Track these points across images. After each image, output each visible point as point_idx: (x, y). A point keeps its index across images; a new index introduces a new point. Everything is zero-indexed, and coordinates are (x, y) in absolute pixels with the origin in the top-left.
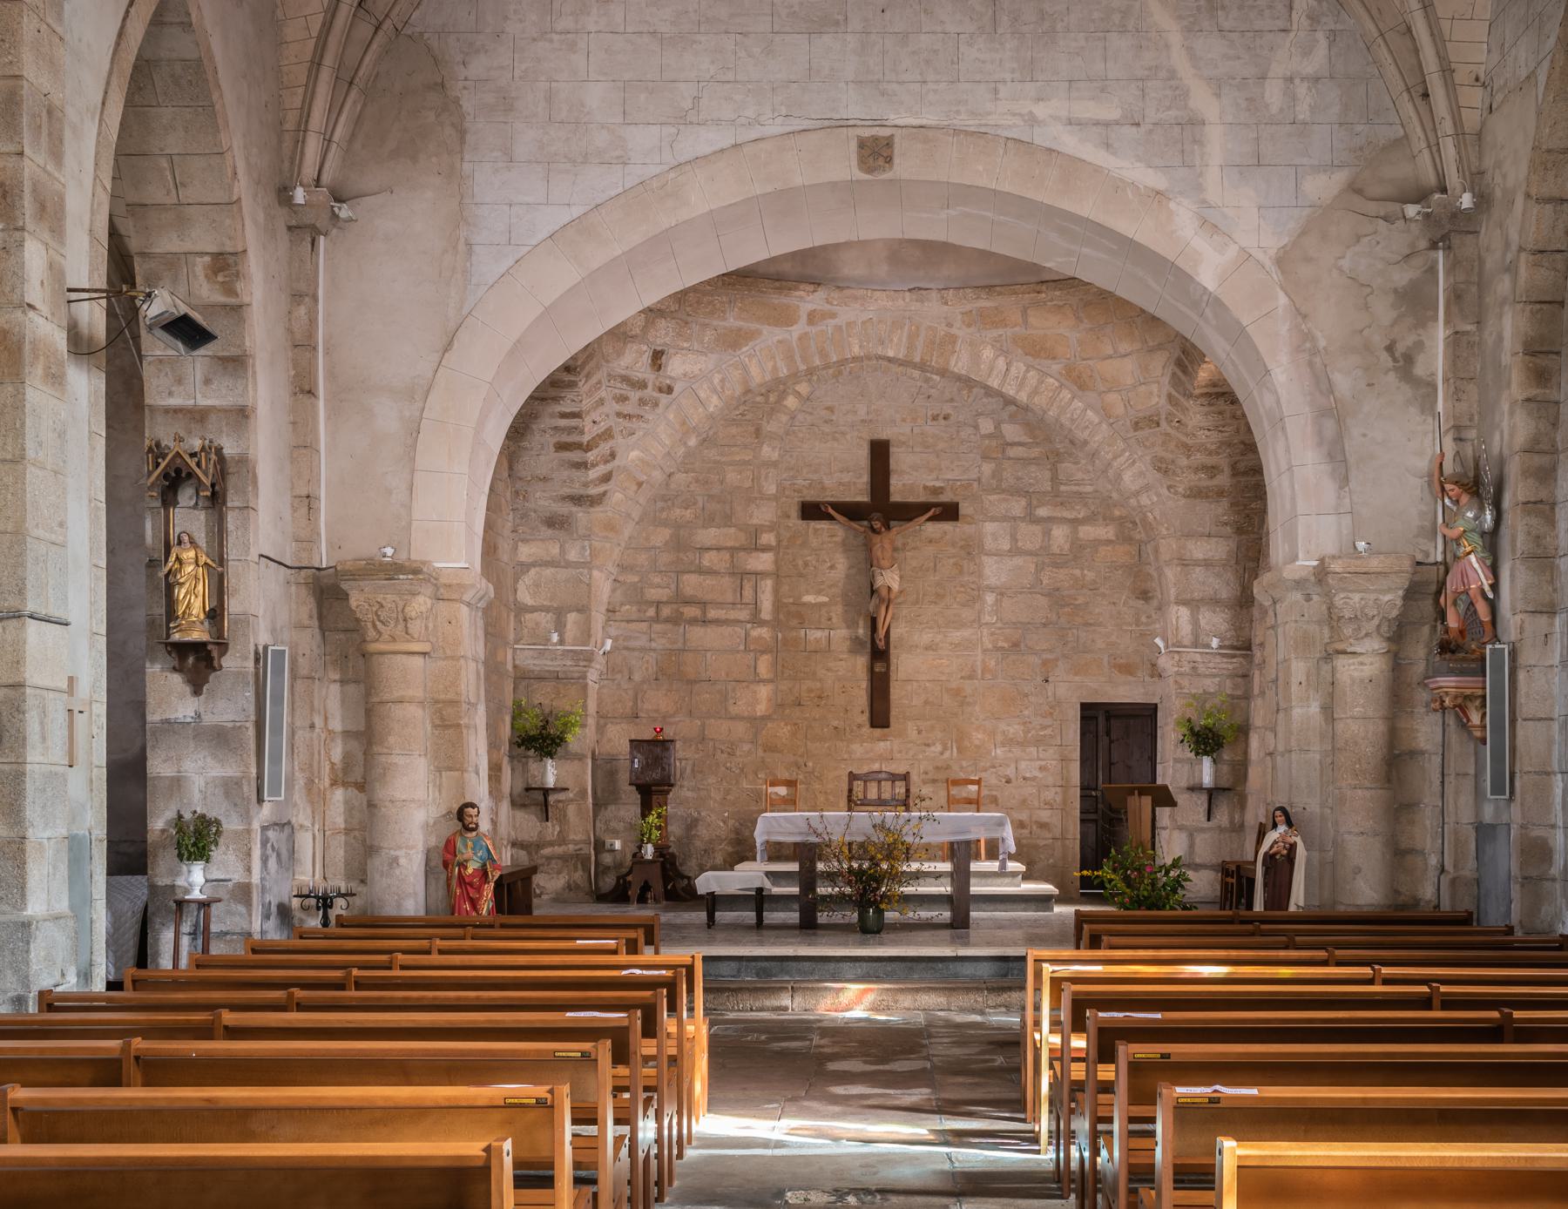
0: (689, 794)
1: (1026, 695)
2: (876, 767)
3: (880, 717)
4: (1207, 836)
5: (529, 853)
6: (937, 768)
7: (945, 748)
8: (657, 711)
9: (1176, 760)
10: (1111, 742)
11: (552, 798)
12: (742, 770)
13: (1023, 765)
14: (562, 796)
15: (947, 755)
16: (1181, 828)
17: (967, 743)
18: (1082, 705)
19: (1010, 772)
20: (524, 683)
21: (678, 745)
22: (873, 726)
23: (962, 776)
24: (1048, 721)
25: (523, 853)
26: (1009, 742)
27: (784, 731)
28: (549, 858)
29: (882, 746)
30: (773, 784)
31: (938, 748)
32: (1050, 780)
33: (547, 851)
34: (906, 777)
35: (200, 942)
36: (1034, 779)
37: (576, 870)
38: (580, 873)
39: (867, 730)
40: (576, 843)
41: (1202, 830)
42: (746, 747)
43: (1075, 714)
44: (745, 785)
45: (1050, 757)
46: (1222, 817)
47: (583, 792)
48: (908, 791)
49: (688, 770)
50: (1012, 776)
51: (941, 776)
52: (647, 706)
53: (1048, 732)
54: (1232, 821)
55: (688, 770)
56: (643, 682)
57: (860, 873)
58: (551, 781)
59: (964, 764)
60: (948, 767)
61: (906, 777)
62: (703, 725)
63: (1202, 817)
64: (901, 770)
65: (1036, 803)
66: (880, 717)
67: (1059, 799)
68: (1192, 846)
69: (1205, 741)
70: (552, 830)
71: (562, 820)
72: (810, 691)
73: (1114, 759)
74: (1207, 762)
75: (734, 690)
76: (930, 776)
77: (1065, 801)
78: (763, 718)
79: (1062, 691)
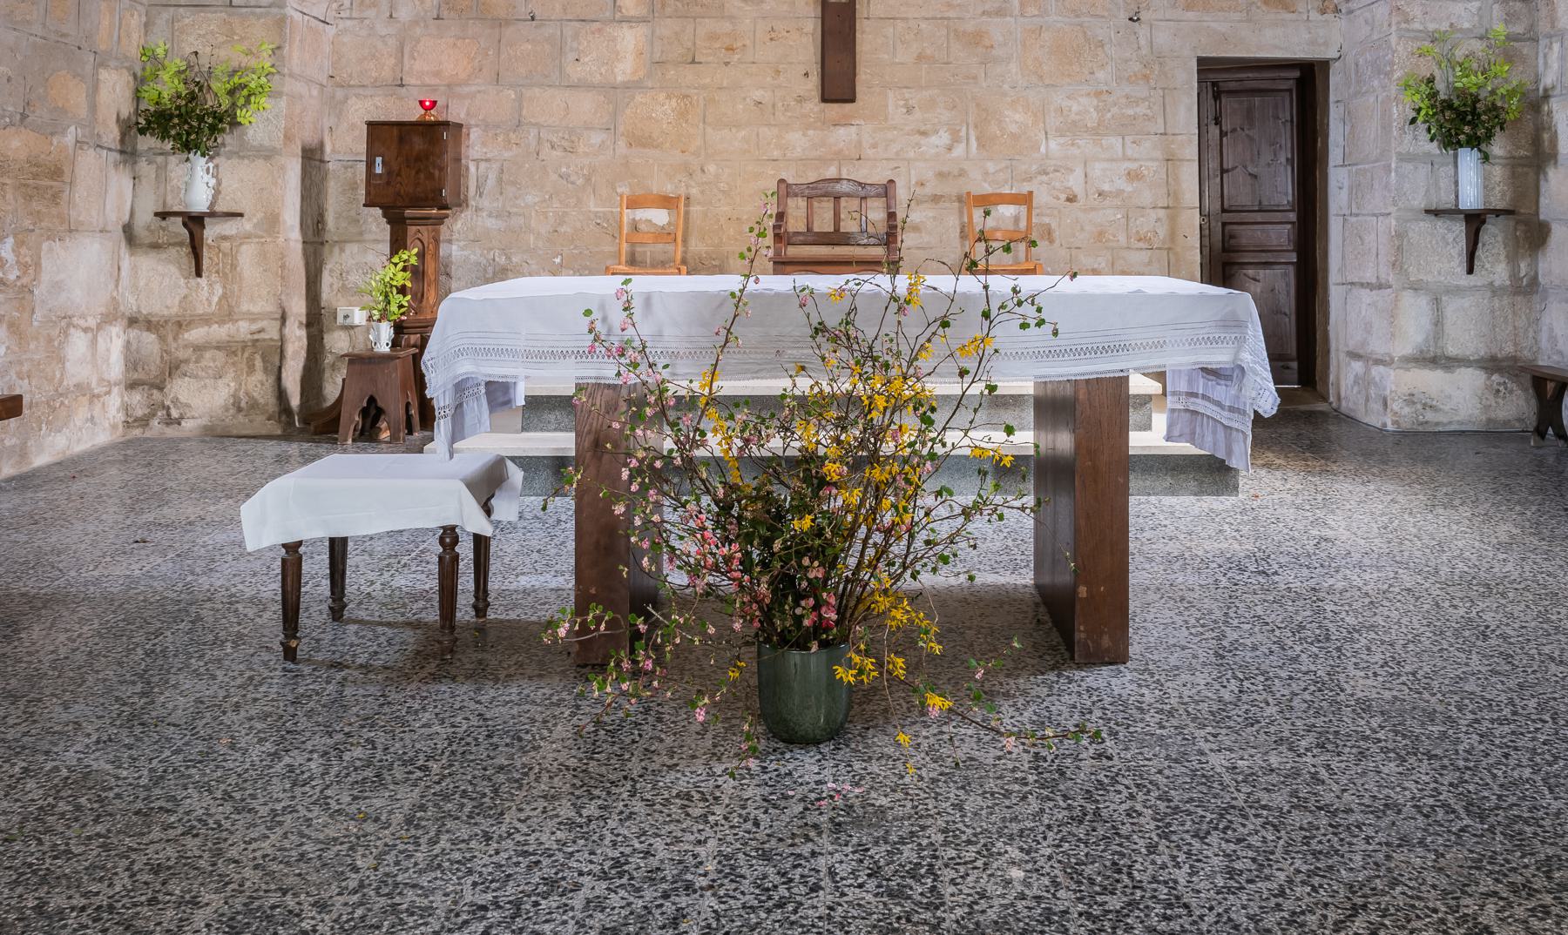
0: (491, 223)
1: (1101, 45)
2: (831, 172)
3: (838, 84)
4: (1466, 302)
5: (162, 339)
6: (941, 175)
7: (956, 139)
8: (437, 74)
9: (1405, 158)
10: (1223, 134)
11: (211, 232)
12: (588, 180)
13: (1097, 169)
14: (230, 227)
15: (959, 150)
16: (1416, 288)
17: (994, 128)
18: (1201, 61)
19: (1075, 182)
20: (166, 15)
21: (475, 134)
22: (824, 100)
23: (987, 189)
24: (1141, 90)
25: (150, 338)
26: (1072, 129)
27: (663, 109)
28: (199, 349)
29: (843, 136)
30: (634, 203)
31: (943, 138)
32: (1147, 197)
33: (196, 335)
34: (887, 191)
35: (1347, 128)
36: (1120, 192)
37: (251, 368)
38: (260, 375)
39: (814, 106)
40: (253, 318)
41: (1457, 291)
42: (596, 138)
43: (1187, 79)
44: (592, 206)
45: (1146, 153)
46: (1495, 266)
47: (272, 222)
48: (892, 216)
49: (491, 182)
50: (1078, 189)
51: (951, 188)
52: (419, 65)
53: (1141, 110)
54: (1514, 276)
55: (491, 181)
56: (415, 23)
57: (802, 497)
58: (199, 201)
59: (991, 167)
60: (962, 173)
61: (887, 191)
62: (520, 98)
63: (1458, 263)
64: (878, 176)
65: (1122, 238)
66: (838, 84)
67: (1162, 232)
68: (1438, 323)
69: (1461, 120)
70: (207, 292)
71: (230, 273)
72: (713, 37)
73: (1228, 164)
74: (1468, 159)
75: (576, 36)
76: (928, 190)
77: (1172, 235)
78: (627, 86)
79: (1163, 38)
